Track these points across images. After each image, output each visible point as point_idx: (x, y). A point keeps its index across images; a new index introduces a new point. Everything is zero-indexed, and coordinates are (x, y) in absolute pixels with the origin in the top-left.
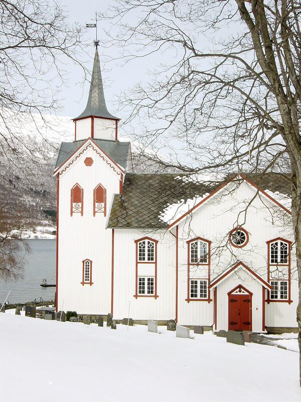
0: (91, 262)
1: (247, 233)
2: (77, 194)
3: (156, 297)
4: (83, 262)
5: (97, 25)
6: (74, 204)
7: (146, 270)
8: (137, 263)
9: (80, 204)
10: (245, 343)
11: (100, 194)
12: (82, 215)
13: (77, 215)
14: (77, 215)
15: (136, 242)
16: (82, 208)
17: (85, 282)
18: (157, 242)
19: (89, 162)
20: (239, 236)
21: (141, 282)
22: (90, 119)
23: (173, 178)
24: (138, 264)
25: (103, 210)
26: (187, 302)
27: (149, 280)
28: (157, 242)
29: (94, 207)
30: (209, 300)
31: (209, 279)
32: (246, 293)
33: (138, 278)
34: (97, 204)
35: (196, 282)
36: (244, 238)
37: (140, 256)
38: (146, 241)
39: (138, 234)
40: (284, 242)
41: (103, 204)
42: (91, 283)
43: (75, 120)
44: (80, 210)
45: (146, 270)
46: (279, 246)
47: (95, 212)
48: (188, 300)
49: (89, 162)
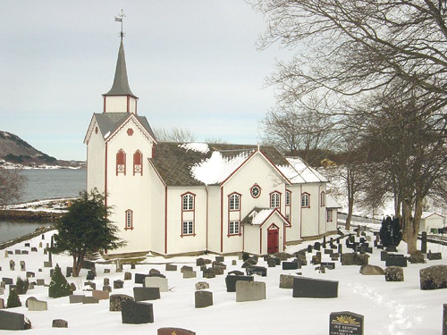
0: (132, 212)
1: (260, 188)
2: (121, 158)
3: (194, 235)
4: (126, 212)
5: (123, 20)
6: (136, 166)
7: (188, 216)
8: (182, 211)
9: (140, 166)
10: (216, 276)
11: (138, 158)
12: (125, 174)
13: (121, 175)
14: (121, 175)
15: (182, 196)
16: (125, 169)
17: (128, 227)
18: (195, 195)
19: (130, 132)
20: (255, 191)
21: (184, 225)
22: (126, 98)
23: (177, 146)
24: (184, 213)
25: (140, 170)
26: (129, 231)
27: (190, 223)
28: (195, 195)
29: (134, 168)
30: (240, 235)
31: (240, 220)
32: (276, 228)
33: (183, 222)
34: (136, 166)
35: (186, 223)
36: (257, 194)
37: (184, 207)
38: (188, 195)
39: (183, 190)
40: (238, 195)
41: (140, 166)
42: (132, 228)
43: (105, 96)
44: (123, 170)
45: (188, 216)
46: (188, 198)
47: (134, 172)
48: (229, 236)
49: (130, 132)
